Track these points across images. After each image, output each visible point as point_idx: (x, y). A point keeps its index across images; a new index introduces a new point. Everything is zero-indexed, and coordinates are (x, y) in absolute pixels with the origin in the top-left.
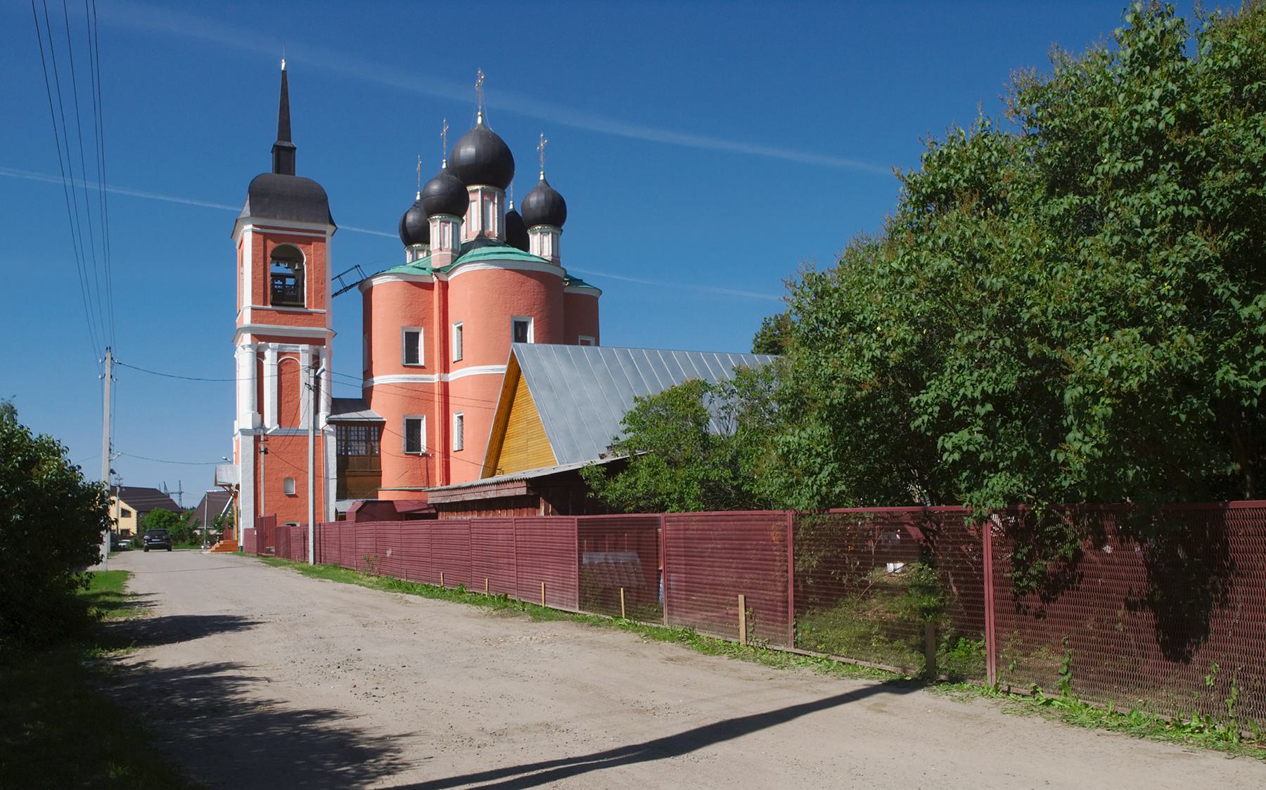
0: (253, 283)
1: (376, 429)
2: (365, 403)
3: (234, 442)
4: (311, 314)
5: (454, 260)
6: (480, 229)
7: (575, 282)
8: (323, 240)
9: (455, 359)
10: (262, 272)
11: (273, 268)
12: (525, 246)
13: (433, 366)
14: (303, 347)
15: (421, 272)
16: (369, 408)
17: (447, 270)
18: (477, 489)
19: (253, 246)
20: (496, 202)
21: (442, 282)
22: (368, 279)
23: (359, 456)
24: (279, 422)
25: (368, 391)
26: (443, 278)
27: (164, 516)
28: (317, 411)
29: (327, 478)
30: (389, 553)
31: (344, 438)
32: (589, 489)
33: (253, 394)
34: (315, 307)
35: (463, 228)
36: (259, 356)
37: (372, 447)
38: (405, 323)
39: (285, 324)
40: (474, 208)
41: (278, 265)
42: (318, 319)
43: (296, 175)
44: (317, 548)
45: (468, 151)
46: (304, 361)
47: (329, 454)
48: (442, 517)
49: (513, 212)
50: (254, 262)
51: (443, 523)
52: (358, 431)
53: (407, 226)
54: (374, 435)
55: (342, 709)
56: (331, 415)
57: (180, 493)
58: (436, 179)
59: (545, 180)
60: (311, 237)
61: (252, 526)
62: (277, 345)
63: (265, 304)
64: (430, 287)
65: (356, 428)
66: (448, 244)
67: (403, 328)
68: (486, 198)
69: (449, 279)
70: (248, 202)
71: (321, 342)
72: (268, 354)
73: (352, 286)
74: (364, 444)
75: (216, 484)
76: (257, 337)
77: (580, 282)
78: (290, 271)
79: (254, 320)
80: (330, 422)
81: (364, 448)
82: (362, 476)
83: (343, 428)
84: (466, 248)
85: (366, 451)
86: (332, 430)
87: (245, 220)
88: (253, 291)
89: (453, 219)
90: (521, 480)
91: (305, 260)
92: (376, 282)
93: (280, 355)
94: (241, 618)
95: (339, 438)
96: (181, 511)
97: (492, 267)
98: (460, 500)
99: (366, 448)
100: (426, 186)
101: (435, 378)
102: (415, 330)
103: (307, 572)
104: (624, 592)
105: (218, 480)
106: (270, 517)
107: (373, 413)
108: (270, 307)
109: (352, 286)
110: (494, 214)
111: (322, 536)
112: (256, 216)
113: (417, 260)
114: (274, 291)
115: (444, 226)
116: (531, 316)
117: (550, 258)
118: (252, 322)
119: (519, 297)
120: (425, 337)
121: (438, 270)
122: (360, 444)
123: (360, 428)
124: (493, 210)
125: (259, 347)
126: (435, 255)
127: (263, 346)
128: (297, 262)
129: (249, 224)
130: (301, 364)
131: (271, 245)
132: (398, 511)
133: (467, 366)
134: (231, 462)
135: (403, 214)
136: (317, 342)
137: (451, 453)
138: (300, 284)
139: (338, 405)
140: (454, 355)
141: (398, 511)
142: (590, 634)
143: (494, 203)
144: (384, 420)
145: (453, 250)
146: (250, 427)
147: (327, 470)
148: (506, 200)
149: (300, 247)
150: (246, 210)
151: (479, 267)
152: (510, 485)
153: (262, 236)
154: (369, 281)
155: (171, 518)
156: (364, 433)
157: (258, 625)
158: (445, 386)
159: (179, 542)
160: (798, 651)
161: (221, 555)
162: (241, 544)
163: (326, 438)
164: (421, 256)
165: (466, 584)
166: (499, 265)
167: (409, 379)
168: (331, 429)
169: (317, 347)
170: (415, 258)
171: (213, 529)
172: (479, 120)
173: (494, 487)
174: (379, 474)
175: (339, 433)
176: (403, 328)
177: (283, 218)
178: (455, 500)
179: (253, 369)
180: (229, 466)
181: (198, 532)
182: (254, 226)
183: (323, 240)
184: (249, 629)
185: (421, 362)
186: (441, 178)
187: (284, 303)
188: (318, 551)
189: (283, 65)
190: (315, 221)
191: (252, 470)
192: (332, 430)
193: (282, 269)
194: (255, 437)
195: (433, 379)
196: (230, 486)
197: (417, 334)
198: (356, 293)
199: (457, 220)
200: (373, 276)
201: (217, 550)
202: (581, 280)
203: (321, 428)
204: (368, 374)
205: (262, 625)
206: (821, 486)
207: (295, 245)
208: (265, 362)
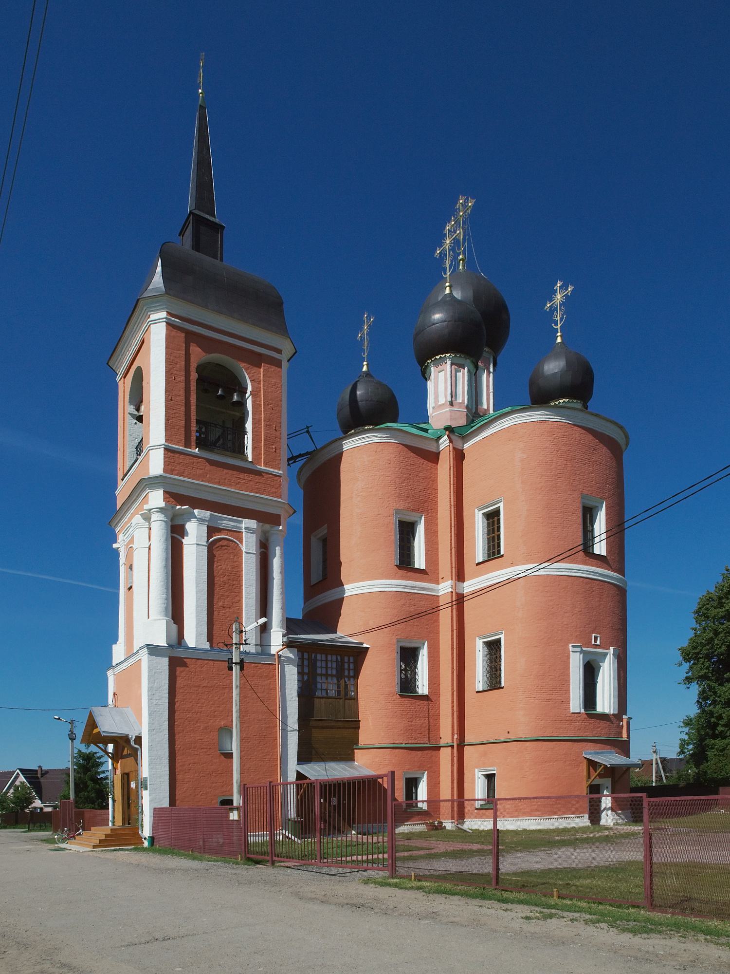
1: (352, 659)
4: (259, 473)
10: (182, 392)
13: (436, 571)
14: (248, 523)
20: (491, 370)
23: (328, 698)
24: (210, 638)
33: (167, 589)
38: (401, 505)
46: (249, 545)
47: (287, 692)
52: (326, 661)
60: (260, 355)
61: (166, 803)
62: (207, 514)
63: (187, 444)
65: (324, 657)
69: (466, 446)
72: (191, 527)
74: (335, 680)
76: (173, 497)
80: (289, 645)
81: (335, 687)
82: (332, 728)
85: (339, 692)
86: (291, 655)
87: (155, 302)
91: (250, 389)
93: (212, 530)
97: (557, 419)
99: (339, 686)
102: (409, 517)
110: (488, 386)
115: (456, 371)
116: (603, 498)
118: (165, 471)
122: (330, 679)
123: (329, 657)
127: (182, 514)
130: (244, 549)
144: (365, 645)
146: (161, 641)
150: (158, 280)
154: (338, 443)
156: (334, 665)
168: (288, 653)
169: (267, 527)
174: (355, 725)
183: (278, 363)
192: (291, 655)
208: (185, 541)
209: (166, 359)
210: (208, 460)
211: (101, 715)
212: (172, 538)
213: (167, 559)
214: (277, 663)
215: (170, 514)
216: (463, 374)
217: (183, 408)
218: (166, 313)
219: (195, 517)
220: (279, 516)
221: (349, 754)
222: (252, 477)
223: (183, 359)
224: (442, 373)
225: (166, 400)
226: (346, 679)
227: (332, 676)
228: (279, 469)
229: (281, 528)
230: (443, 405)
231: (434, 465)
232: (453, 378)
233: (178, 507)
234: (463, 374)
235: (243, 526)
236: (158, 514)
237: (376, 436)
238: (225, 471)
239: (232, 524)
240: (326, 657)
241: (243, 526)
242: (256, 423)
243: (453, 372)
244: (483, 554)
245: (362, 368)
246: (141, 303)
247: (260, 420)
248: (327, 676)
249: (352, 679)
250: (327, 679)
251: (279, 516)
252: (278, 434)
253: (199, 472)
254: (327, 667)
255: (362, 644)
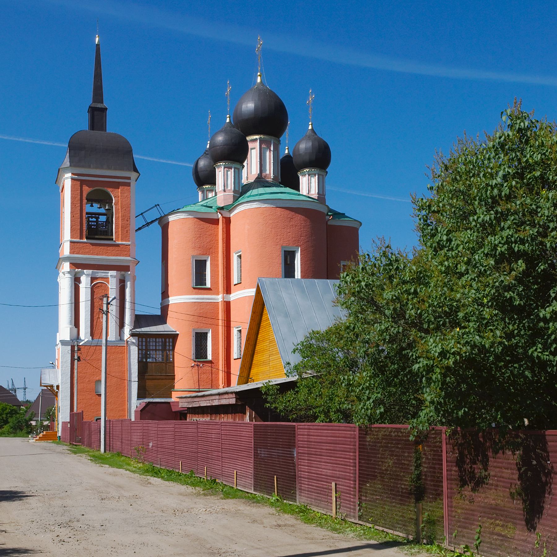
0: (71, 221)
1: (171, 340)
2: (162, 319)
3: (57, 351)
4: (118, 245)
5: (236, 199)
6: (259, 172)
7: (337, 215)
8: (128, 185)
9: (235, 282)
10: (79, 212)
11: (88, 208)
12: (296, 186)
15: (209, 210)
16: (165, 323)
17: (230, 208)
18: (208, 398)
19: (71, 191)
21: (225, 217)
22: (165, 215)
24: (92, 334)
25: (165, 309)
26: (226, 215)
27: (6, 409)
28: (121, 325)
29: (130, 381)
30: (151, 444)
31: (144, 348)
32: (266, 401)
33: (71, 311)
34: (122, 240)
35: (244, 171)
36: (76, 281)
37: (167, 356)
38: (196, 253)
39: (97, 255)
40: (254, 155)
41: (92, 206)
42: (125, 249)
43: (107, 131)
44: (108, 439)
45: (249, 106)
47: (132, 360)
48: (192, 418)
49: (288, 157)
50: (73, 204)
51: (192, 423)
53: (199, 170)
54: (169, 346)
55: (28, 548)
56: (134, 329)
57: (25, 389)
58: (221, 131)
59: (312, 129)
63: (81, 238)
64: (215, 222)
65: (154, 340)
66: (231, 186)
67: (193, 257)
68: (263, 146)
69: (231, 215)
70: (68, 154)
71: (126, 268)
73: (152, 222)
74: (161, 353)
75: (41, 386)
76: (75, 265)
77: (343, 215)
78: (102, 211)
79: (72, 251)
80: (133, 335)
81: (160, 356)
83: (144, 340)
84: (246, 188)
85: (163, 359)
86: (134, 341)
87: (66, 170)
88: (71, 227)
89: (234, 165)
90: (232, 393)
91: (114, 202)
92: (171, 218)
93: (93, 279)
94: (20, 492)
95: (140, 347)
96: (19, 404)
97: (266, 205)
98: (198, 406)
99: (163, 356)
100: (212, 139)
101: (219, 298)
102: (203, 258)
103: (98, 459)
104: (277, 478)
105: (43, 382)
106: (78, 413)
107: (169, 327)
108: (85, 240)
109: (152, 222)
110: (270, 159)
111: (111, 430)
112: (75, 166)
113: (207, 199)
114: (89, 227)
115: (227, 171)
116: (298, 246)
117: (315, 196)
118: (70, 253)
119: (288, 231)
120: (211, 264)
121: (222, 208)
123: (157, 340)
124: (269, 156)
125: (76, 273)
126: (220, 195)
128: (107, 203)
129: (69, 173)
130: (110, 287)
131: (87, 190)
132: (173, 411)
133: (244, 288)
134: (54, 367)
135: (196, 160)
136: (122, 268)
137: (232, 361)
138: (110, 220)
139: (139, 320)
140: (235, 279)
141: (173, 411)
142: (248, 508)
143: (270, 150)
144: (178, 332)
145: (235, 191)
146: (68, 339)
147: (130, 374)
148: (281, 147)
149: (109, 190)
151: (255, 205)
152: (226, 396)
153: (79, 182)
154: (166, 218)
155: (12, 410)
156: (160, 343)
157: (28, 498)
158: (228, 305)
159: (18, 431)
160: (360, 522)
161: (43, 444)
162: (59, 434)
163: (130, 348)
164: (210, 195)
165: (195, 471)
166: (271, 204)
167: (198, 299)
169: (123, 273)
170: (205, 198)
171: (46, 421)
172: (259, 80)
173: (217, 397)
174: (172, 378)
175: (140, 343)
176: (193, 257)
177: (96, 168)
178: (195, 406)
179: (71, 291)
180: (51, 370)
181: (34, 423)
182: (73, 174)
183: (128, 185)
184: (20, 500)
185: (208, 285)
186: (224, 131)
187: (96, 237)
188: (108, 442)
189: (97, 39)
190: (122, 169)
191: (69, 374)
192: (134, 341)
193: (96, 208)
194: (72, 346)
195: (218, 299)
196: (52, 386)
197: (205, 261)
198: (156, 228)
199: (238, 166)
200: (172, 212)
201: (41, 439)
202: (344, 214)
203: (125, 339)
204: (165, 294)
205: (31, 498)
206: (367, 409)
207: (105, 189)
208: (81, 285)
209: (71, 197)
210: (91, 244)
211: (44, 374)
212: (75, 283)
213: (71, 297)
214: (126, 345)
215: (74, 274)
216: (231, 172)
217: (79, 220)
218: (71, 174)
219: (85, 274)
220: (129, 266)
221: (169, 394)
222: (114, 248)
223: (79, 195)
224: (220, 172)
225: (71, 217)
226: (168, 351)
227: (159, 350)
228: (129, 241)
229: (129, 273)
230: (221, 191)
231: (216, 226)
232: (225, 176)
233: (77, 270)
234: (231, 172)
235: (109, 274)
236: (68, 274)
237: (182, 215)
238: (100, 247)
239: (104, 274)
240: (156, 340)
241: (109, 274)
242: (117, 219)
243: (225, 172)
244: (238, 279)
245: (226, 120)
246: (60, 170)
247: (119, 217)
248: (156, 350)
249: (171, 351)
250: (156, 352)
251: (129, 266)
252: (128, 222)
253: (87, 250)
254: (156, 346)
255: (176, 331)
